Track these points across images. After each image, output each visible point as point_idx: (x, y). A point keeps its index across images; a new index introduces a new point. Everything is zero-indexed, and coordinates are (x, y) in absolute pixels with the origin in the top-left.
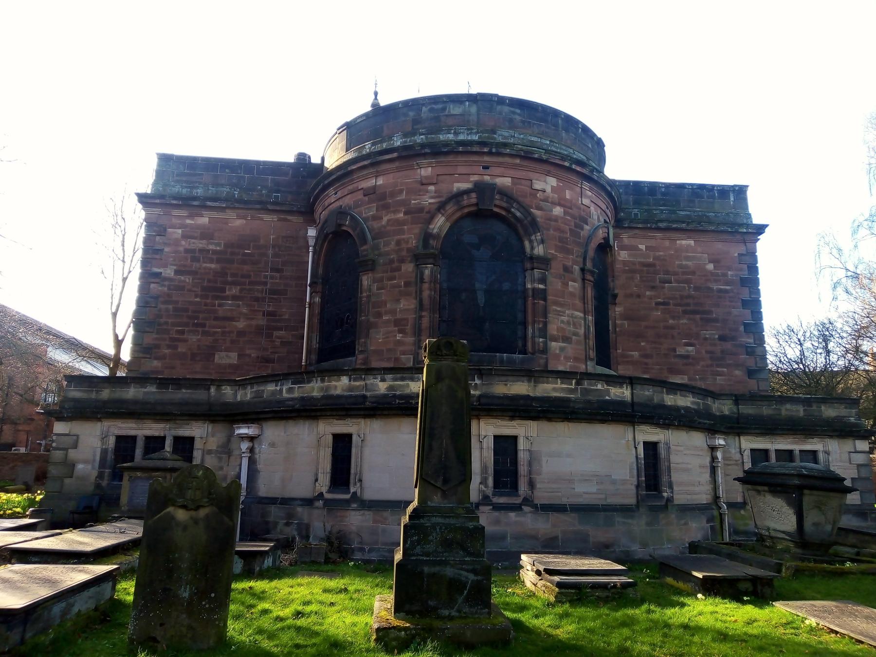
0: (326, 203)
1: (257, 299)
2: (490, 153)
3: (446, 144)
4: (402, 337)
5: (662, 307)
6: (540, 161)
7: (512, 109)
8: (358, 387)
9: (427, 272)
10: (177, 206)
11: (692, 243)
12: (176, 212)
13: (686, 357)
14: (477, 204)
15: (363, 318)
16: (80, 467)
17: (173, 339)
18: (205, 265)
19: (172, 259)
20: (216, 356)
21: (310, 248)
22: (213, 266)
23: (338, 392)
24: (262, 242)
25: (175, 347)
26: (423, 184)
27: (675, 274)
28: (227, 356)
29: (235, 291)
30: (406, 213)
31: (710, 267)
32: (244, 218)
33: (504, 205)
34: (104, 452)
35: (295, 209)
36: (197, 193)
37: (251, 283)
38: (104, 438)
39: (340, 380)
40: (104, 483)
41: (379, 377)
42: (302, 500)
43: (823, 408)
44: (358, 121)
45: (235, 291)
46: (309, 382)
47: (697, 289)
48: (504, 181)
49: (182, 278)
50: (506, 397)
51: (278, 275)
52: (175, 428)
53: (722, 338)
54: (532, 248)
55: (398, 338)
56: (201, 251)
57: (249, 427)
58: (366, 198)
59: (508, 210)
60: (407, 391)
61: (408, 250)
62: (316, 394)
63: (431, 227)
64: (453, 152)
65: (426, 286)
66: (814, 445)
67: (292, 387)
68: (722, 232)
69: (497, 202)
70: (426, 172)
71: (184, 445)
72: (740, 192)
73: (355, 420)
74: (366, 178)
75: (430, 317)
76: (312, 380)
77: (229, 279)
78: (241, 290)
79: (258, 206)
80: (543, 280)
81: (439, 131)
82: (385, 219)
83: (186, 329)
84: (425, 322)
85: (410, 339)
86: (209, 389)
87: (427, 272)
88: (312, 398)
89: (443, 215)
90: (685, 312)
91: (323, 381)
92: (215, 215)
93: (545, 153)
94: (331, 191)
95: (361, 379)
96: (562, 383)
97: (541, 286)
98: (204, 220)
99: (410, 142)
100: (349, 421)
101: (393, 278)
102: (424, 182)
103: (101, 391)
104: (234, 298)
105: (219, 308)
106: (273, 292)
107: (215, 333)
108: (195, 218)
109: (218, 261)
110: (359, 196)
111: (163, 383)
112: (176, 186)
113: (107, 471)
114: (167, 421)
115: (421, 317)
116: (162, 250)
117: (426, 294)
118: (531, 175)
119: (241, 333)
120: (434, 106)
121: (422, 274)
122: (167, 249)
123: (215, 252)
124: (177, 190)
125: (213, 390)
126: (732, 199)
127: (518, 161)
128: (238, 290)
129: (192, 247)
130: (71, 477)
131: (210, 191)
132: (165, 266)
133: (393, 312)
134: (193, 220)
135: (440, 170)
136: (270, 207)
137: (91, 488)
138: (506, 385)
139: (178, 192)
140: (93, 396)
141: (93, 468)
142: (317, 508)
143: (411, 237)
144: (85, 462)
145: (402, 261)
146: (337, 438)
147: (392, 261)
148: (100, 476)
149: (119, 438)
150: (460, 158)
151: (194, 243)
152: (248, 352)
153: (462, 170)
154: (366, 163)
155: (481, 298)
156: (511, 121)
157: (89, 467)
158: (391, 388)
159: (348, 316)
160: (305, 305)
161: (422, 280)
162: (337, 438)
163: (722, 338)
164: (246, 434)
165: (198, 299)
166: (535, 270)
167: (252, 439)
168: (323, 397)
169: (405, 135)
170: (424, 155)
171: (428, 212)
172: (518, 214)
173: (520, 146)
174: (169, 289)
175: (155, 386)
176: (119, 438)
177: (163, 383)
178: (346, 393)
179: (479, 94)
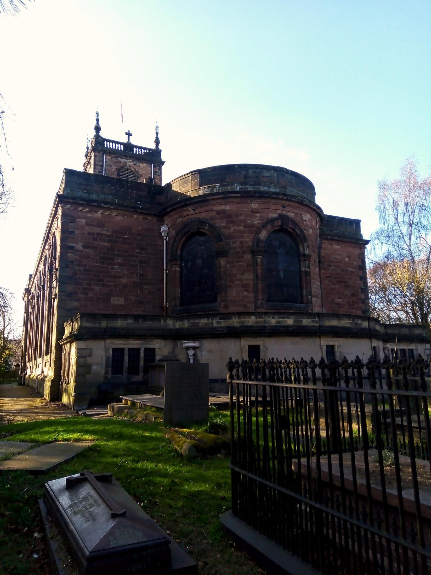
0: (185, 214)
2: (287, 200)
3: (267, 193)
5: (329, 279)
6: (306, 206)
7: (292, 177)
8: (261, 321)
9: (259, 260)
10: (82, 205)
11: (339, 247)
12: (81, 209)
13: (339, 304)
14: (281, 226)
15: (222, 282)
16: (94, 367)
17: (84, 289)
18: (101, 243)
19: (80, 238)
20: (112, 299)
21: (164, 237)
22: (106, 244)
23: (250, 324)
24: (134, 231)
26: (253, 212)
27: (334, 262)
28: (118, 300)
29: (120, 260)
30: (245, 227)
31: (347, 259)
32: (123, 215)
33: (293, 227)
34: (107, 358)
35: (153, 213)
36: (93, 198)
38: (106, 351)
39: (250, 318)
40: (109, 376)
41: (271, 316)
43: (415, 330)
44: (208, 170)
45: (120, 260)
47: (342, 270)
48: (291, 215)
49: (88, 251)
50: (330, 327)
51: (144, 252)
53: (353, 295)
54: (304, 250)
55: (245, 294)
56: (98, 234)
57: (195, 342)
58: (219, 216)
59: (294, 230)
60: (286, 324)
61: (248, 247)
62: (236, 325)
63: (260, 236)
64: (270, 197)
65: (259, 267)
66: (413, 346)
67: (220, 321)
68: (352, 243)
69: (290, 226)
70: (255, 206)
71: (150, 352)
72: (357, 223)
73: (261, 338)
74: (218, 204)
75: (262, 284)
76: (232, 318)
79: (132, 210)
80: (309, 267)
81: (260, 184)
82: (232, 230)
83: (93, 282)
84: (260, 286)
85: (252, 295)
86: (160, 321)
87: (259, 260)
88: (234, 327)
89: (266, 230)
90: (338, 282)
91: (239, 318)
92: (105, 212)
93: (308, 202)
94: (191, 208)
95: (262, 317)
96: (348, 320)
97: (308, 270)
98: (98, 215)
100: (258, 339)
101: (240, 262)
104: (120, 264)
108: (93, 213)
109: (109, 241)
110: (214, 214)
111: (137, 318)
112: (80, 191)
113: (110, 369)
115: (257, 283)
116: (74, 232)
117: (259, 271)
118: (303, 213)
120: (256, 170)
121: (257, 261)
122: (77, 232)
123: (106, 236)
124: (80, 194)
125: (162, 321)
126: (354, 226)
127: (297, 205)
130: (90, 374)
131: (101, 197)
132: (76, 242)
133: (241, 280)
134: (91, 214)
136: (139, 211)
137: (102, 379)
138: (329, 321)
139: (81, 195)
140: (97, 325)
143: (248, 240)
144: (97, 364)
145: (244, 252)
146: (250, 347)
147: (238, 252)
148: (107, 372)
149: (114, 350)
150: (273, 201)
151: (93, 229)
152: (130, 297)
153: (273, 207)
154: (220, 196)
155: (282, 275)
156: (291, 182)
157: (100, 367)
158: (278, 322)
159: (205, 281)
160: (163, 271)
161: (257, 264)
162: (250, 347)
163: (353, 295)
164: (194, 346)
165: (98, 264)
166: (306, 261)
167: (194, 348)
168: (241, 327)
169: (242, 184)
170: (254, 197)
171: (257, 228)
172: (298, 232)
173: (300, 198)
174: (80, 257)
175: (132, 320)
176: (114, 350)
177: (137, 318)
178: (255, 325)
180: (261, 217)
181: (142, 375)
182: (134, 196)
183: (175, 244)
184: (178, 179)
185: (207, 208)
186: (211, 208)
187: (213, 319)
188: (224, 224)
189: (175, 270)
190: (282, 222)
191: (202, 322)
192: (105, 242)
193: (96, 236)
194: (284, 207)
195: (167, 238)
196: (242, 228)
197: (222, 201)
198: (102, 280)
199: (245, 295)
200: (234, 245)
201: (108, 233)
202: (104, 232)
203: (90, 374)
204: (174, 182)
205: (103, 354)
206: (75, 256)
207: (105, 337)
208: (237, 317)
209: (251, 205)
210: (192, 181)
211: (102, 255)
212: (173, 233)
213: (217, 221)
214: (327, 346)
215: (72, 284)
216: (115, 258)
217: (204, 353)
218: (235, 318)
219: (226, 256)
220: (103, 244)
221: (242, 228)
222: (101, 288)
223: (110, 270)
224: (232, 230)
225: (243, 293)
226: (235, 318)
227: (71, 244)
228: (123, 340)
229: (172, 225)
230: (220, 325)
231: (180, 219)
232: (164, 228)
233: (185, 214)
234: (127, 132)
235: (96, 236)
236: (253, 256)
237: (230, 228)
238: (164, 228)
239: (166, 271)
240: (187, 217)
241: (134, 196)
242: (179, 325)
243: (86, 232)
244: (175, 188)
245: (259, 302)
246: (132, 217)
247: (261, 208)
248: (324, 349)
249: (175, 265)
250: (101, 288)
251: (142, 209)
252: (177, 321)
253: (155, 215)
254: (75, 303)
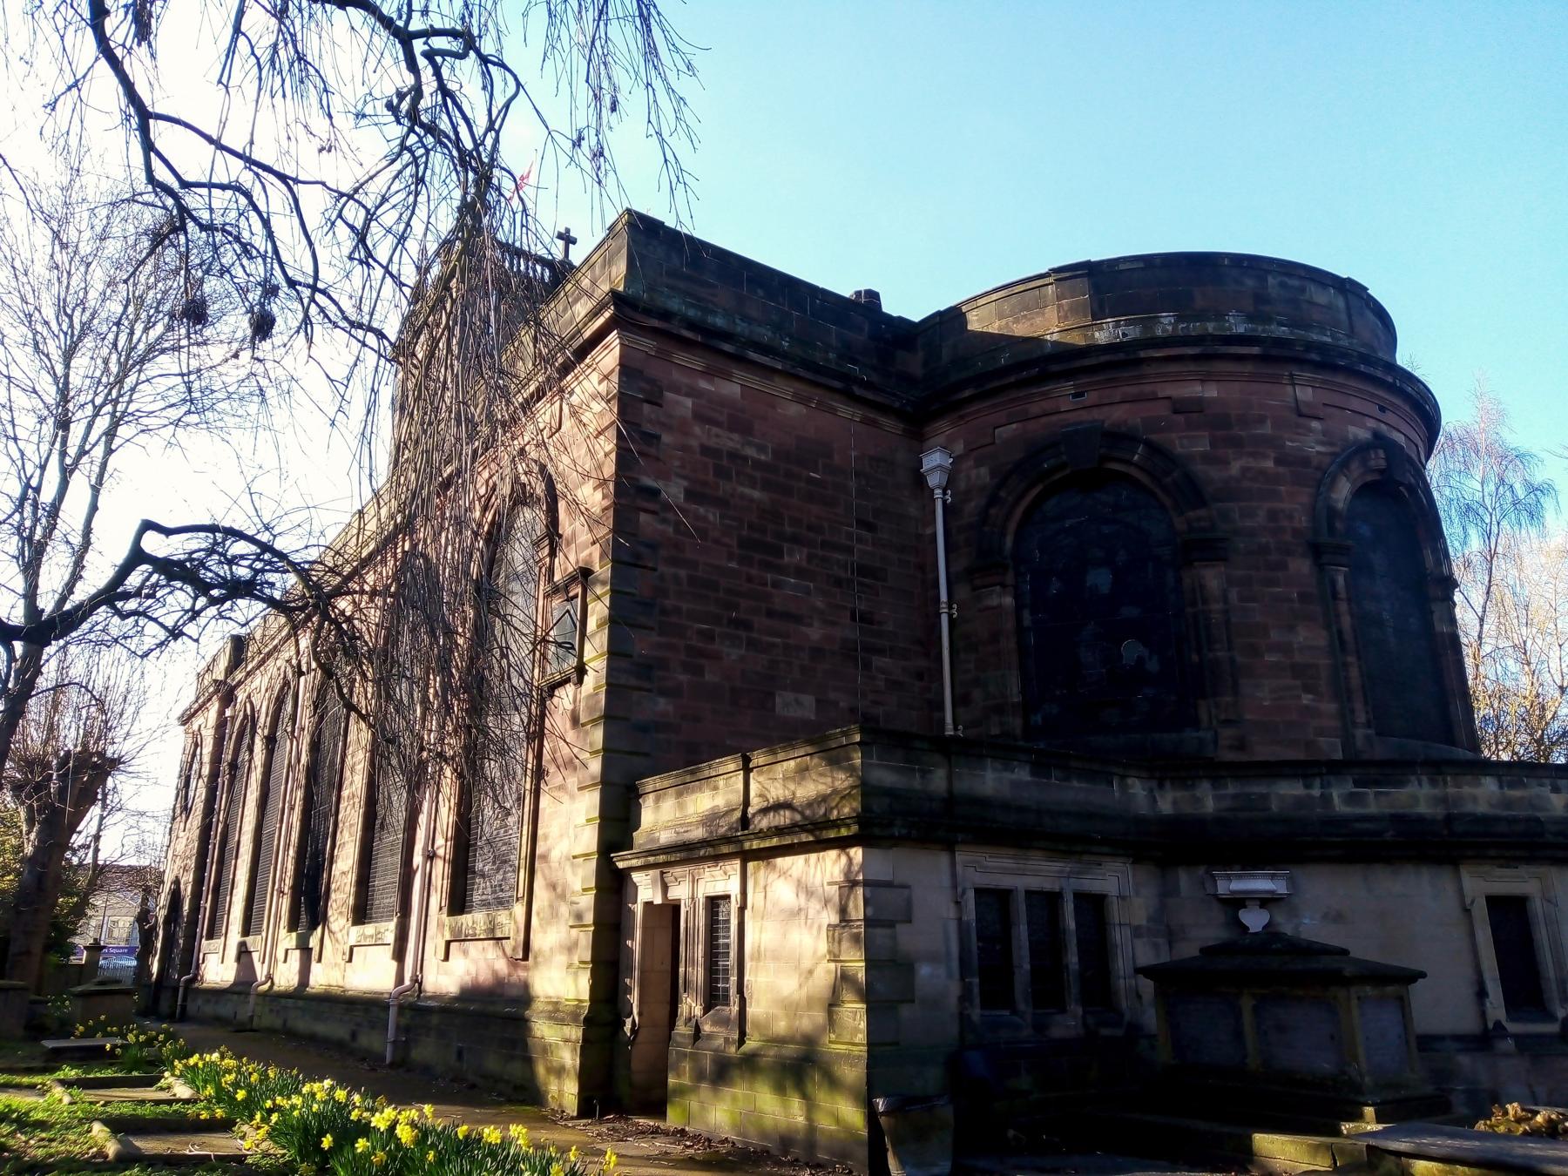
0: (1035, 409)
1: (838, 583)
4: (1313, 700)
9: (1341, 580)
12: (682, 358)
16: (924, 971)
18: (741, 489)
20: (778, 700)
22: (756, 494)
23: (1482, 808)
25: (697, 671)
26: (1300, 415)
30: (1278, 462)
37: (824, 544)
39: (1479, 784)
42: (1457, 1038)
44: (1122, 267)
46: (1400, 784)
49: (702, 510)
52: (1079, 873)
55: (1305, 702)
56: (734, 456)
57: (1273, 877)
58: (1180, 418)
61: (1296, 532)
62: (1423, 809)
63: (1334, 496)
70: (1305, 394)
73: (1533, 869)
77: (788, 529)
78: (810, 557)
79: (837, 384)
82: (1235, 468)
83: (718, 630)
87: (1341, 580)
91: (1433, 783)
92: (755, 381)
94: (1068, 387)
99: (1264, 331)
100: (1523, 870)
102: (1305, 410)
103: (930, 771)
104: (800, 573)
105: (774, 591)
106: (863, 570)
107: (774, 645)
109: (766, 485)
110: (1162, 410)
114: (1066, 854)
116: (658, 438)
119: (817, 652)
121: (1333, 583)
122: (666, 438)
123: (757, 464)
128: (804, 557)
129: (712, 443)
132: (664, 475)
134: (711, 382)
135: (1329, 397)
136: (857, 390)
140: (916, 783)
141: (950, 975)
142: (1507, 1055)
143: (1296, 505)
144: (933, 958)
146: (1496, 904)
148: (965, 997)
151: (717, 436)
152: (832, 695)
153: (1356, 404)
157: (942, 971)
161: (1335, 596)
162: (1496, 904)
164: (1272, 892)
165: (733, 565)
169: (1250, 318)
170: (1300, 362)
171: (1318, 468)
175: (1028, 768)
179: (1349, 280)
180: (1325, 433)
181: (1080, 1011)
182: (834, 342)
183: (993, 511)
184: (994, 297)
185: (1132, 390)
186: (1147, 389)
187: (1329, 785)
188: (1202, 446)
189: (1000, 606)
190: (1387, 459)
191: (1282, 792)
192: (754, 487)
193: (725, 462)
194: (1382, 409)
195: (945, 493)
196: (1269, 464)
197: (1192, 367)
198: (747, 626)
199: (1307, 707)
200: (1248, 523)
201: (763, 457)
202: (750, 452)
203: (913, 1001)
204: (974, 305)
205: (952, 913)
206: (660, 527)
207: (960, 837)
208: (1424, 778)
209: (1289, 388)
210: (1059, 298)
211: (745, 533)
212: (982, 475)
213: (1174, 435)
214: (980, 892)
215: (652, 629)
216: (786, 546)
217: (1306, 921)
218: (1420, 784)
219: (1225, 559)
220: (747, 491)
221: (1269, 464)
222: (743, 652)
223: (769, 588)
224: (1235, 468)
225: (1299, 697)
226: (1420, 784)
227: (648, 481)
228: (1012, 852)
229: (972, 450)
230: (1359, 811)
231: (1014, 426)
232: (935, 461)
233: (1035, 409)
234: (563, 231)
235: (725, 462)
236: (1320, 566)
237: (1225, 463)
238: (935, 461)
239: (950, 607)
240: (1044, 420)
241: (834, 342)
242: (1175, 803)
243: (694, 443)
244: (976, 322)
245: (1360, 733)
246: (833, 411)
247: (1324, 404)
248: (1481, 912)
249: (998, 588)
250: (743, 652)
251: (868, 386)
252: (1161, 786)
253: (899, 414)
254: (663, 704)
